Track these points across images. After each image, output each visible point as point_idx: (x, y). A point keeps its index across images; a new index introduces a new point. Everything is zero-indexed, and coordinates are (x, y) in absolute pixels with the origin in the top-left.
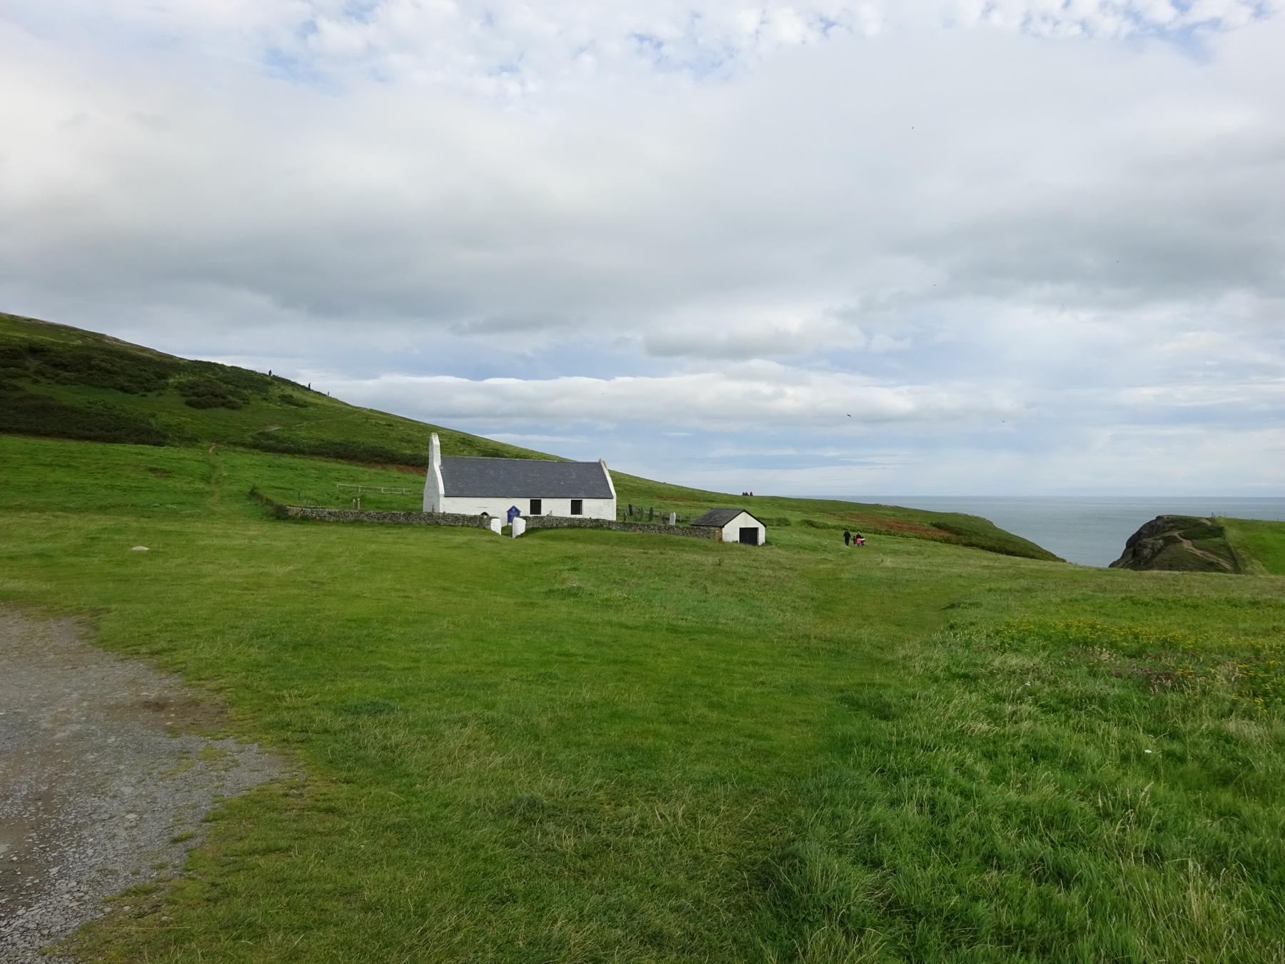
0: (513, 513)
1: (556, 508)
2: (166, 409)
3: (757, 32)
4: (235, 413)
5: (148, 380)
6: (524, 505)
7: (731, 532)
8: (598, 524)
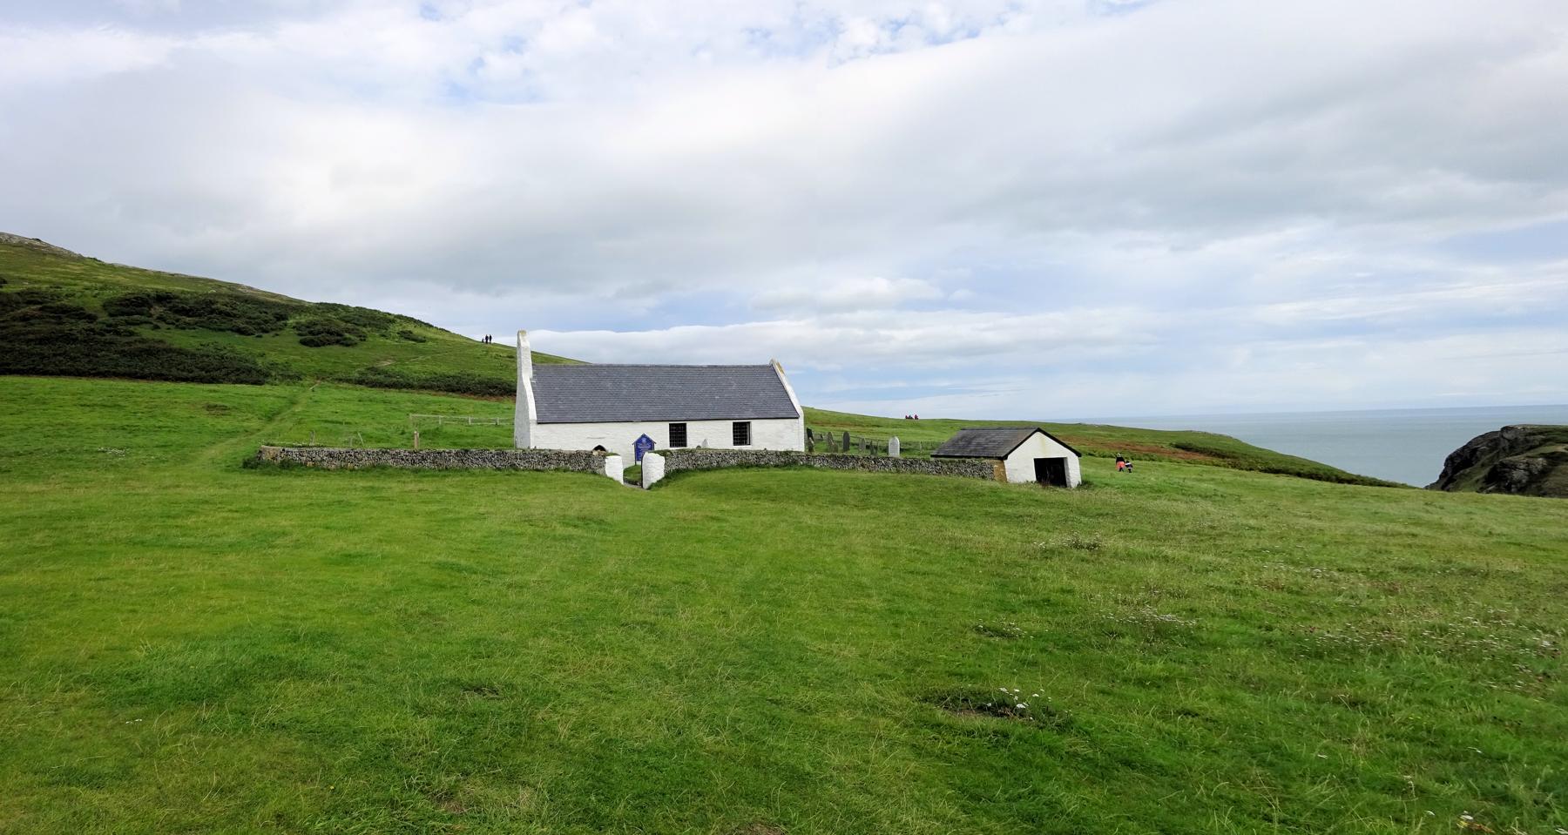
0: (643, 446)
1: (710, 435)
2: (280, 349)
4: (350, 350)
5: (266, 322)
6: (660, 434)
7: (1020, 466)
8: (787, 460)
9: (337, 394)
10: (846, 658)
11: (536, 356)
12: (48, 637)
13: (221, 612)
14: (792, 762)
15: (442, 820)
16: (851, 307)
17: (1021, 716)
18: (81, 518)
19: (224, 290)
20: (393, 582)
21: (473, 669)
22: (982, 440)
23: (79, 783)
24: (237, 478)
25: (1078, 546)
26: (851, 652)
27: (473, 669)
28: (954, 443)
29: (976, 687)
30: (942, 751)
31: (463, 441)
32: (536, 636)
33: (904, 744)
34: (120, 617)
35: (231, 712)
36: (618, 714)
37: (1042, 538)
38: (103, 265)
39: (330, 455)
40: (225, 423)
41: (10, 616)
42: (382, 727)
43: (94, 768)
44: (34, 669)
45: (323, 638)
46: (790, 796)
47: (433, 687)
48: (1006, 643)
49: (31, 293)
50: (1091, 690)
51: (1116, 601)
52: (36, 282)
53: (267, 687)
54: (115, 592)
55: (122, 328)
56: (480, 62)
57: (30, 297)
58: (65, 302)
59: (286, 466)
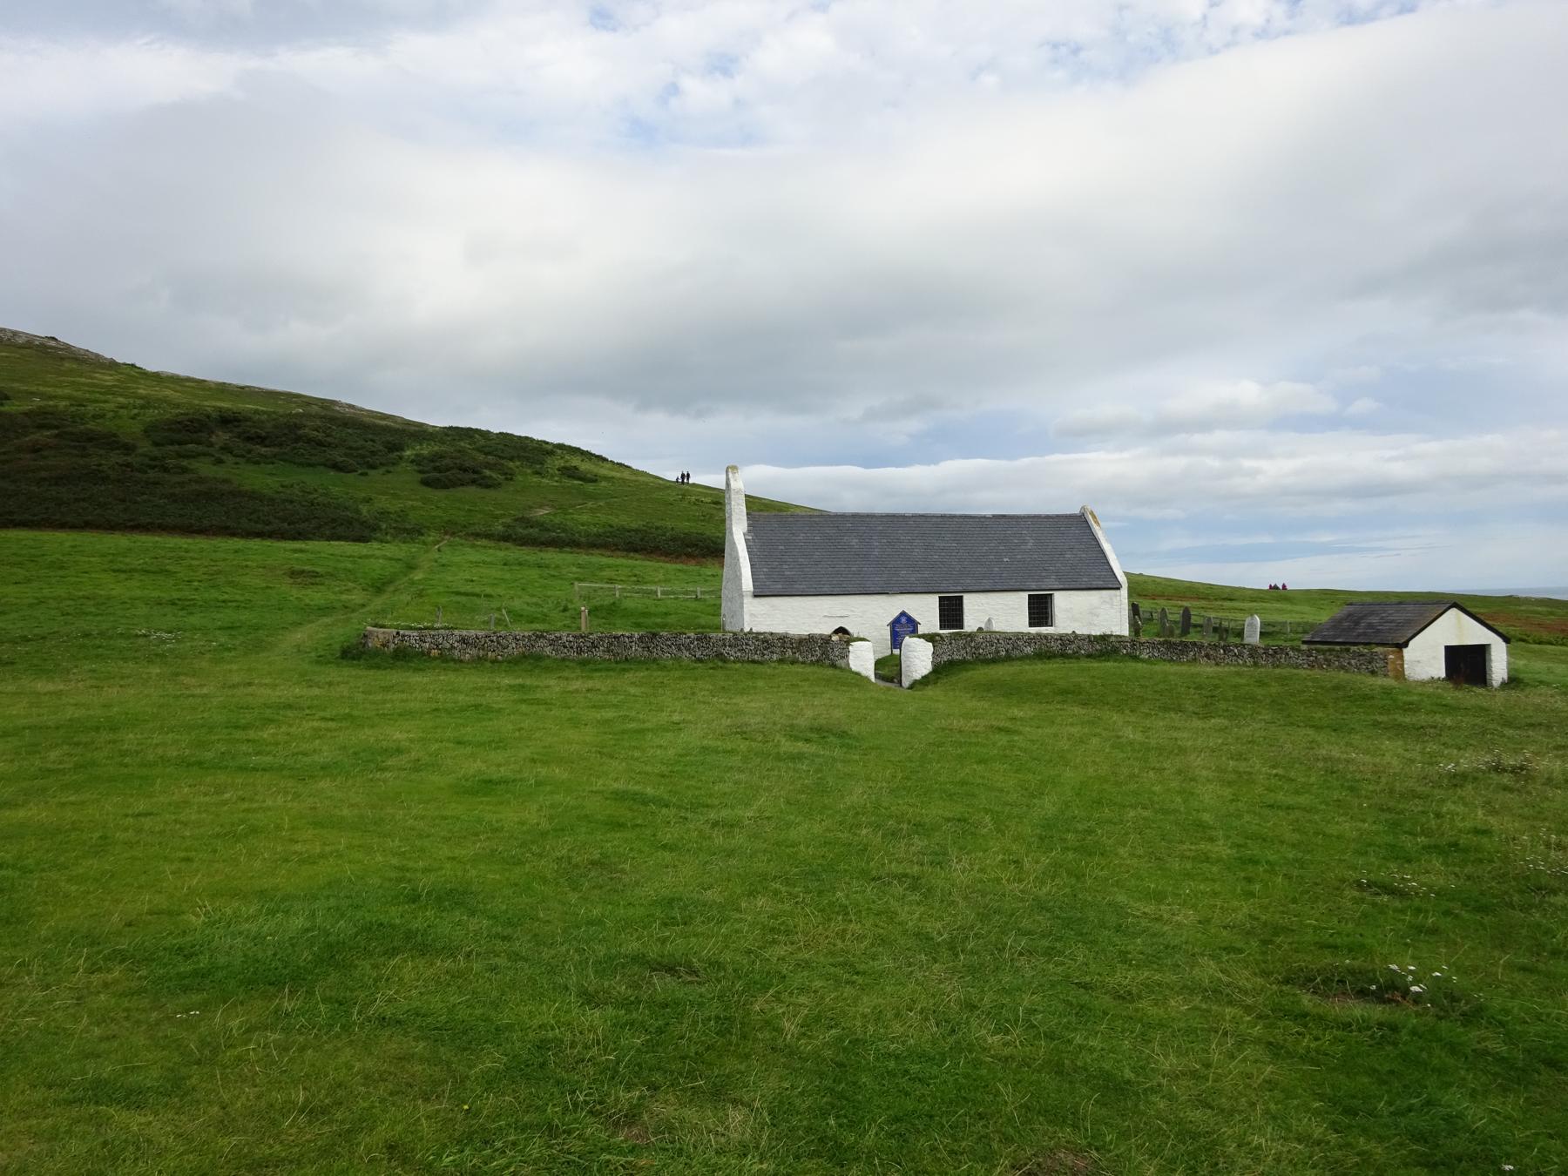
0: (903, 626)
1: (997, 612)
2: (393, 492)
3: (1205, 17)
4: (491, 493)
6: (926, 611)
7: (1425, 657)
8: (1104, 647)
9: (474, 556)
10: (1179, 925)
11: (752, 503)
12: (66, 896)
13: (311, 860)
14: (1107, 1066)
15: (621, 1153)
16: (1205, 424)
17: (1416, 1002)
18: (114, 729)
19: (315, 409)
20: (551, 818)
21: (664, 941)
22: (1374, 620)
23: (112, 1101)
24: (333, 673)
25: (1498, 769)
26: (1188, 917)
27: (664, 941)
28: (1336, 624)
29: (1356, 963)
30: (1308, 1050)
31: (649, 621)
32: (752, 894)
33: (1257, 1041)
34: (168, 868)
35: (324, 1001)
36: (867, 1004)
37: (1450, 759)
38: (144, 374)
39: (463, 640)
40: (315, 596)
41: (14, 867)
42: (536, 1022)
43: (132, 1079)
44: (47, 940)
45: (453, 898)
46: (1104, 1112)
47: (607, 966)
48: (1397, 904)
49: (43, 412)
50: (1509, 966)
51: (1548, 845)
52: (51, 398)
53: (375, 967)
54: (162, 832)
55: (171, 462)
56: (673, 89)
57: (42, 419)
58: (91, 426)
59: (402, 656)
